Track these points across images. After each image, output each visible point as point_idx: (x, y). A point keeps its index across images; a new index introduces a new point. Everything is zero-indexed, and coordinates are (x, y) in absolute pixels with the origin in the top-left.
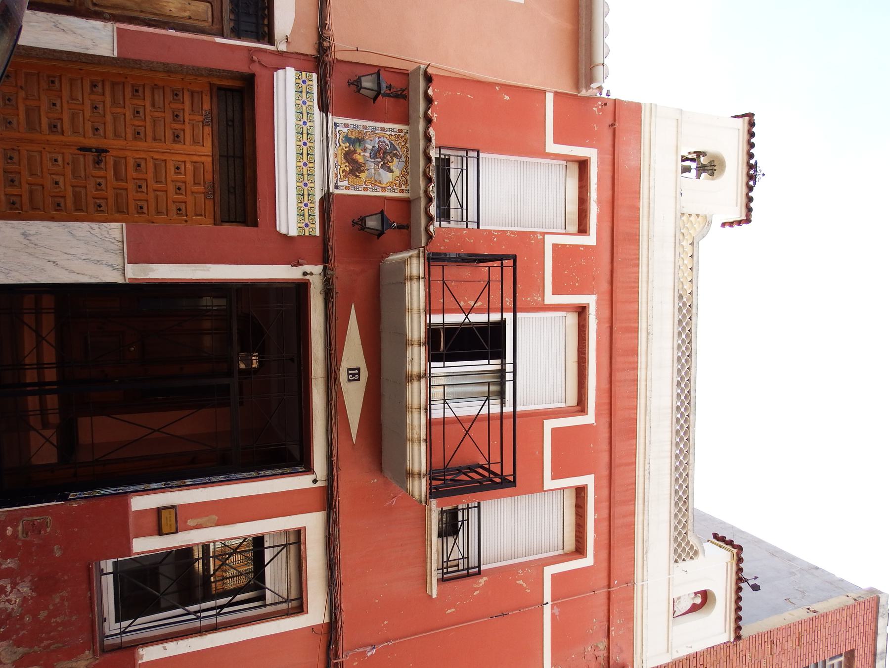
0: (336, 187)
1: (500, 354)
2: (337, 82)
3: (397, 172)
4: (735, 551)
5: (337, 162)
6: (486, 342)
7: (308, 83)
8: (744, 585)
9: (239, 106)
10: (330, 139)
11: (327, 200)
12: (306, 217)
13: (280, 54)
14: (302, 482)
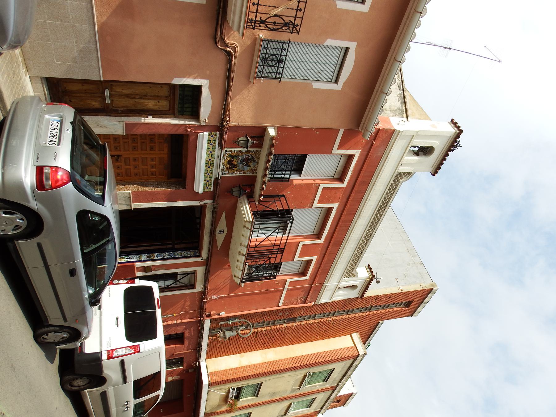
0: (222, 174)
2: (226, 138)
3: (252, 166)
4: (458, 131)
9: (178, 149)
11: (216, 181)
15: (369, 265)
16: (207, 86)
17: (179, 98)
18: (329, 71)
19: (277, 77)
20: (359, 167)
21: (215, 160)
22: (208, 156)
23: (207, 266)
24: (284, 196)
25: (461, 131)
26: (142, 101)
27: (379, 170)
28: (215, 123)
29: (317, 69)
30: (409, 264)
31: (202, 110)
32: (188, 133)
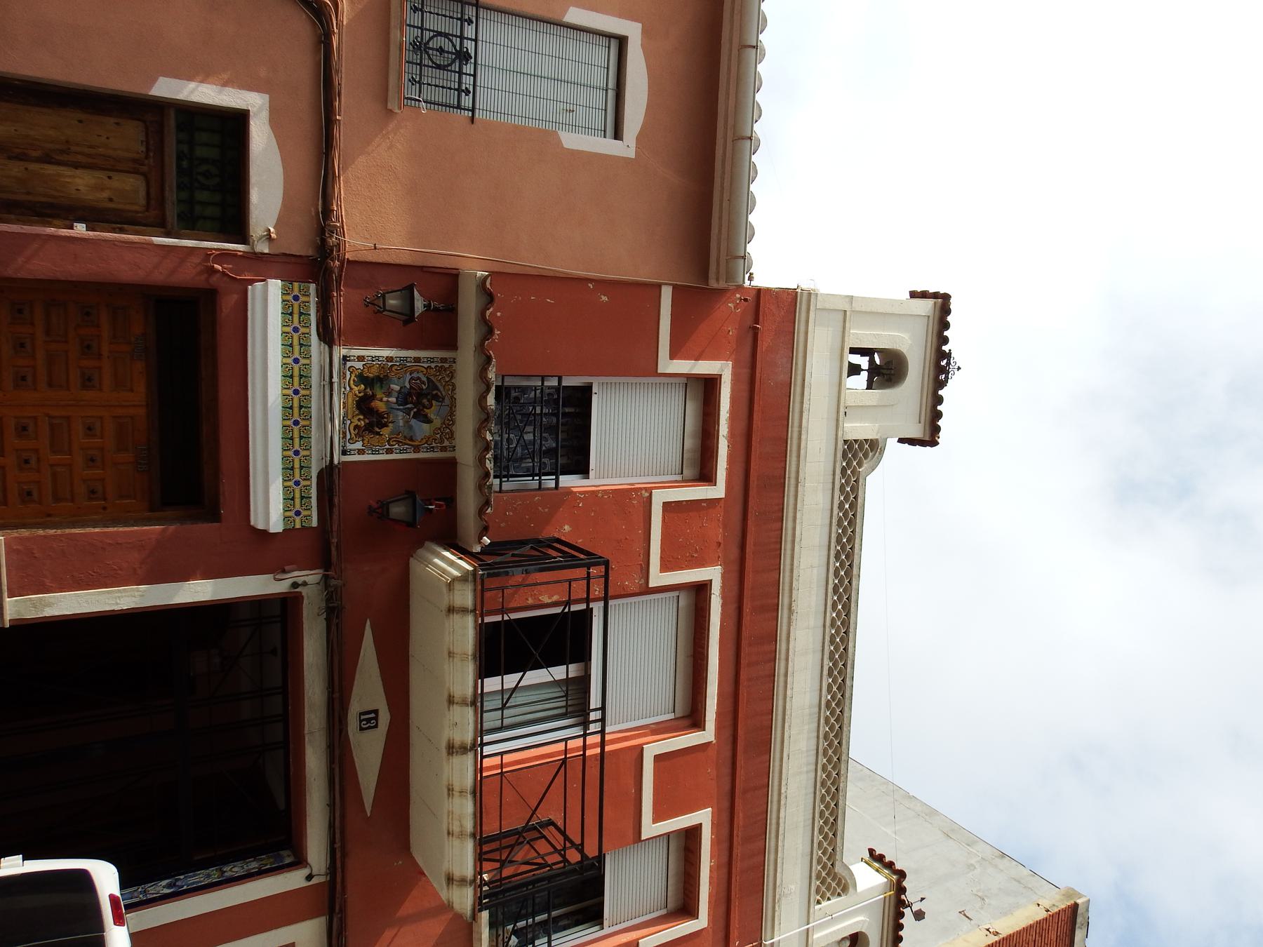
0: (344, 453)
1: (583, 656)
2: (343, 299)
3: (437, 422)
5: (346, 415)
6: (565, 639)
7: (302, 299)
8: (907, 911)
9: (188, 342)
10: (336, 386)
11: (329, 475)
12: (297, 501)
13: (256, 258)
14: (292, 881)
15: (871, 851)
16: (265, 114)
17: (179, 166)
18: (596, 102)
19: (461, 98)
20: (743, 424)
21: (315, 392)
22: (288, 376)
23: (331, 913)
24: (551, 823)
25: (902, 875)
26: (51, 169)
27: (796, 429)
28: (299, 246)
29: (558, 93)
30: (971, 867)
31: (255, 196)
32: (214, 279)
